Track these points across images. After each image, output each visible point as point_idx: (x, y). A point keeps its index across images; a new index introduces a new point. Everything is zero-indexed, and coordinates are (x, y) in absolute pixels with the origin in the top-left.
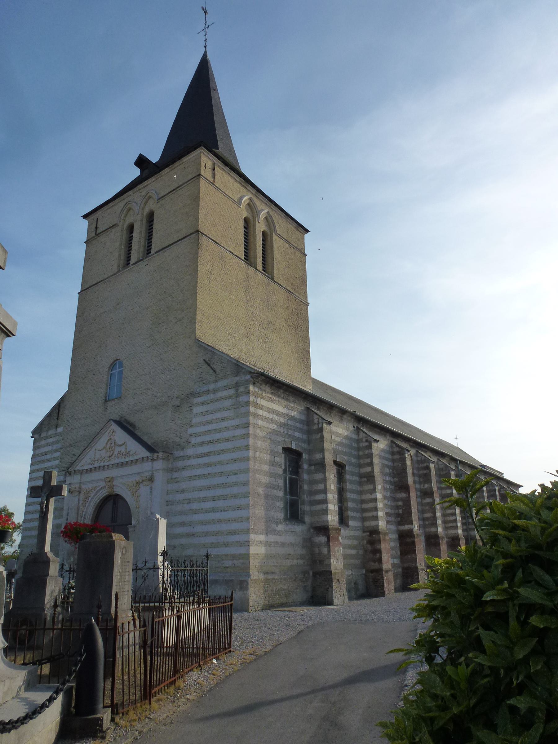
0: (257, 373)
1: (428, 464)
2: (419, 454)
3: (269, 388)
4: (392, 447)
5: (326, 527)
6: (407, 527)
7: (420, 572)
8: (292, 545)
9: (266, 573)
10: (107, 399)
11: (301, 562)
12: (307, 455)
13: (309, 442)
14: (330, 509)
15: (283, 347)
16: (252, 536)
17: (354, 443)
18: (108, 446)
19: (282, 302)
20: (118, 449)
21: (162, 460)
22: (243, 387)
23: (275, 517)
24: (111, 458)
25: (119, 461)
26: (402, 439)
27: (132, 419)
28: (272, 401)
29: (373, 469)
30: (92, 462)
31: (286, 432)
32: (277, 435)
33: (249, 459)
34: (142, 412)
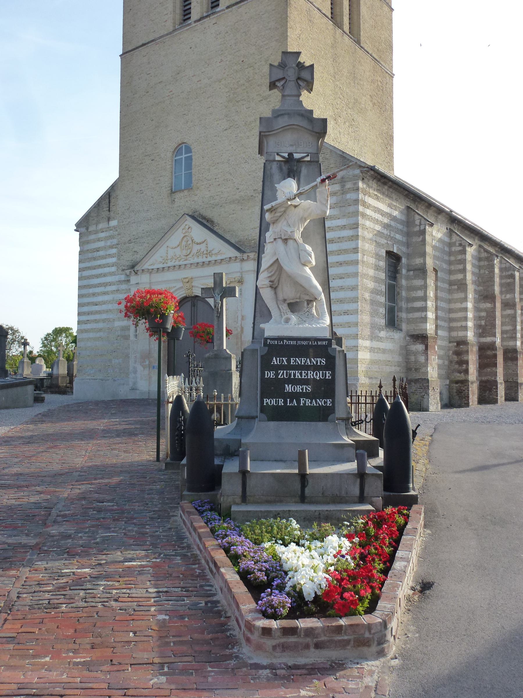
0: (367, 167)
1: (513, 272)
2: (503, 260)
3: (376, 184)
4: (479, 252)
5: (424, 335)
6: (488, 339)
7: (499, 386)
8: (391, 351)
9: (370, 378)
10: (173, 190)
11: (398, 369)
12: (406, 259)
13: (408, 245)
14: (429, 317)
15: (368, 131)
16: (360, 341)
17: (446, 247)
18: (184, 243)
19: (368, 74)
20: (196, 248)
21: (253, 261)
22: (351, 182)
23: (379, 324)
24: (188, 257)
25: (200, 260)
26: (489, 243)
27: (209, 213)
28: (377, 198)
29: (465, 276)
30: (164, 261)
31: (389, 234)
32: (381, 237)
33: (358, 262)
34: (221, 206)
